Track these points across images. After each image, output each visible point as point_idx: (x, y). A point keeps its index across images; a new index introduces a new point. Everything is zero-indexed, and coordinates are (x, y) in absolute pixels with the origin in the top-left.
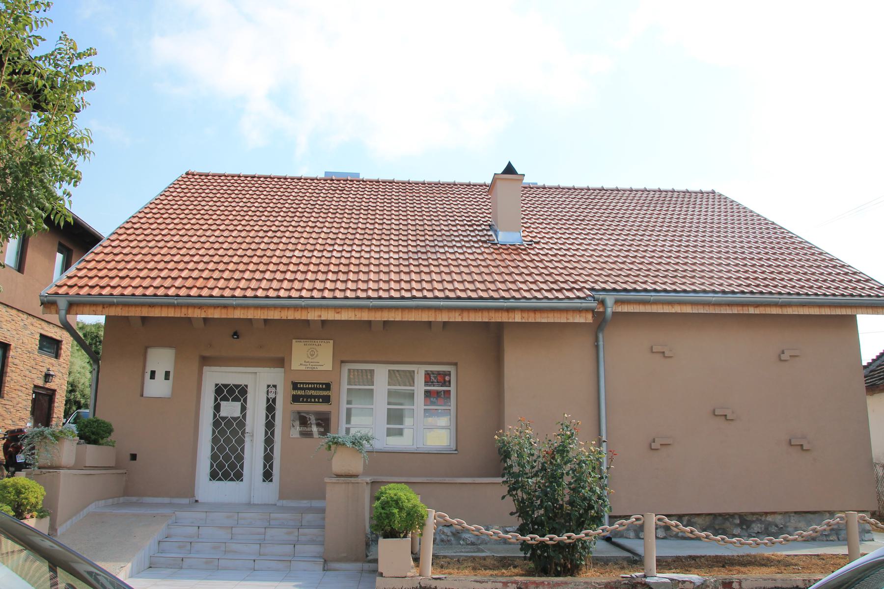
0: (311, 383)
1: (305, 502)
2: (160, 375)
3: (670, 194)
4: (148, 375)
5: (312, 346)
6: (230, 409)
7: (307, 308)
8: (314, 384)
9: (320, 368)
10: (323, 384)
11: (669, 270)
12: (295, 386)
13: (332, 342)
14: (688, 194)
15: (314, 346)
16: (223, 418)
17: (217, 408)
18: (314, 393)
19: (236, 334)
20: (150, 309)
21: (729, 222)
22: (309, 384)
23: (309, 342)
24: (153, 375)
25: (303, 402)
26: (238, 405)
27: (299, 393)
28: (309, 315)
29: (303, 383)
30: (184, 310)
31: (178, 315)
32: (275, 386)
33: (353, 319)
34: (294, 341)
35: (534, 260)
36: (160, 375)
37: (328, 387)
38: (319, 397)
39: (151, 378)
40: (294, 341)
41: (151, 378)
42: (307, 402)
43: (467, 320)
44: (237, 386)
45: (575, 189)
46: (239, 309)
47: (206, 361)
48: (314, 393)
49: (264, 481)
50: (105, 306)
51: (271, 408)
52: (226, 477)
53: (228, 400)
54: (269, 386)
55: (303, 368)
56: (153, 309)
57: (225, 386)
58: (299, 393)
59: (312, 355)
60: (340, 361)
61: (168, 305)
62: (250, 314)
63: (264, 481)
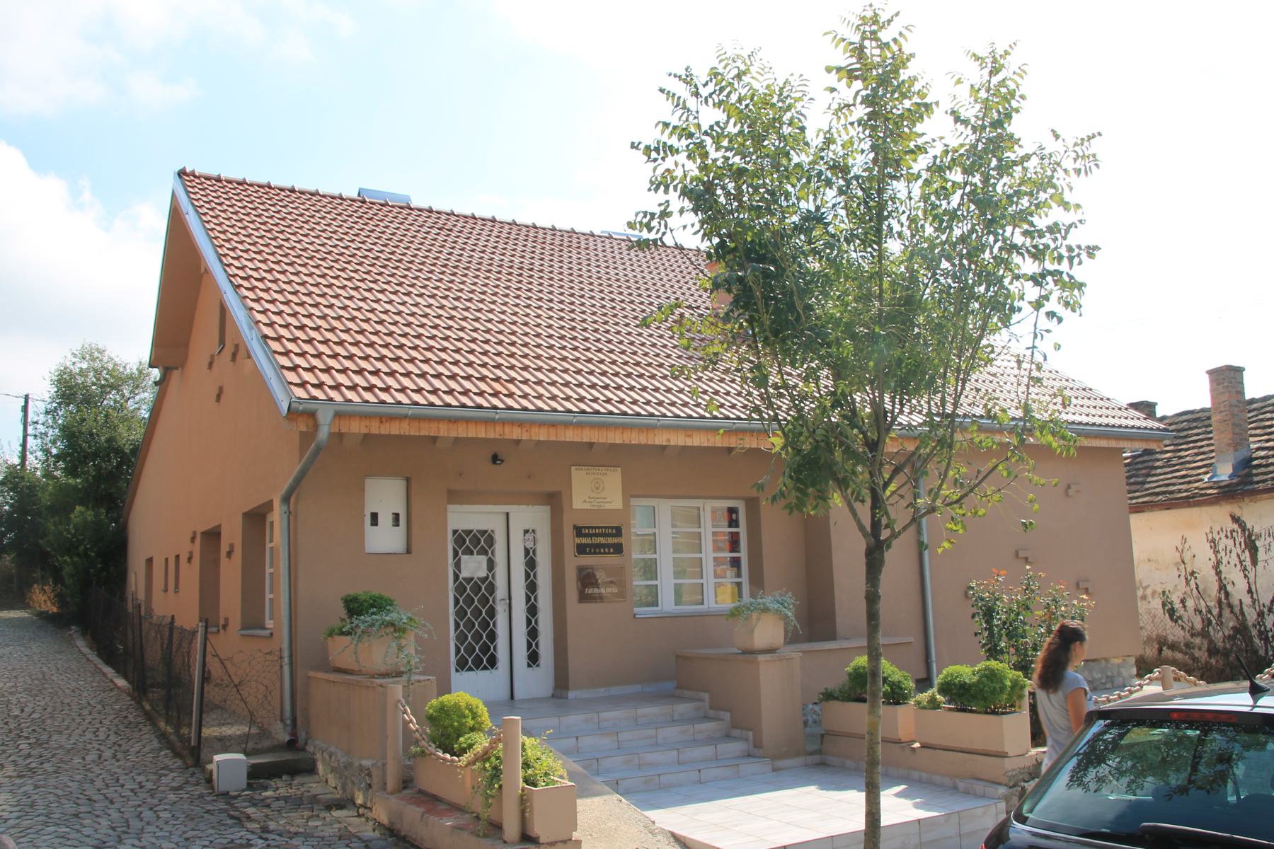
0: (599, 528)
1: (603, 690)
2: (385, 519)
3: (443, 217)
4: (368, 520)
5: (596, 476)
6: (474, 566)
7: (504, 424)
8: (602, 528)
9: (608, 506)
10: (612, 528)
11: (408, 334)
12: (579, 531)
13: (619, 469)
14: (515, 228)
15: (599, 476)
16: (469, 580)
17: (491, 565)
18: (602, 540)
19: (495, 459)
20: (450, 425)
21: (506, 264)
22: (596, 528)
23: (592, 470)
24: (375, 518)
25: (590, 553)
26: (483, 559)
27: (586, 541)
28: (657, 438)
29: (588, 528)
30: (499, 429)
31: (414, 432)
32: (533, 531)
33: (706, 445)
34: (573, 468)
35: (268, 310)
36: (385, 519)
37: (618, 532)
38: (609, 546)
39: (372, 525)
40: (573, 468)
41: (372, 525)
42: (595, 553)
43: (554, 439)
44: (483, 532)
45: (341, 198)
46: (571, 428)
47: (455, 497)
48: (602, 540)
49: (529, 666)
50: (384, 420)
51: (531, 564)
52: (478, 664)
53: (472, 553)
54: (526, 532)
55: (587, 506)
56: (455, 426)
57: (468, 532)
58: (586, 541)
59: (597, 488)
60: (630, 492)
61: (477, 421)
62: (516, 433)
63: (529, 666)
